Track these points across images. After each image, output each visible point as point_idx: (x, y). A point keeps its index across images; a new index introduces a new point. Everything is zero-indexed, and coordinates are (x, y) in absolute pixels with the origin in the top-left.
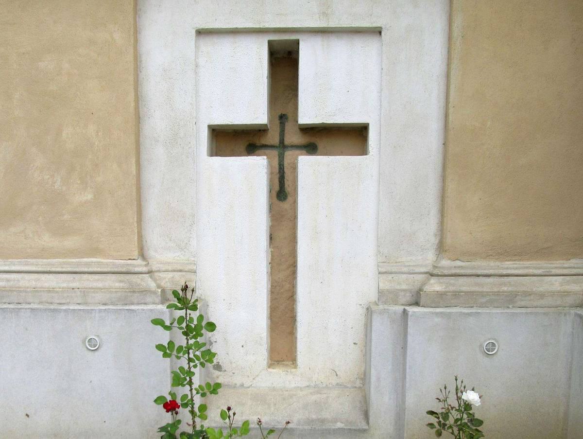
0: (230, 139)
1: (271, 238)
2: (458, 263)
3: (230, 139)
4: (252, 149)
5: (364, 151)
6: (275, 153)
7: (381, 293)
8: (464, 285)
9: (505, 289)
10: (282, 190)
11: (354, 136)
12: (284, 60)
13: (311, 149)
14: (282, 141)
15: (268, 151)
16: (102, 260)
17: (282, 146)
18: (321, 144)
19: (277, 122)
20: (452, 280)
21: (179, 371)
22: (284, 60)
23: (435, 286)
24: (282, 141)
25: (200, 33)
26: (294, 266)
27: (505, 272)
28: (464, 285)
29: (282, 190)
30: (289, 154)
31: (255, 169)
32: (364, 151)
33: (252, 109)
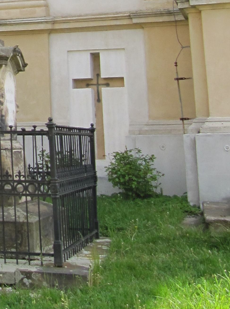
0: (79, 83)
1: (96, 115)
2: (155, 121)
3: (79, 83)
4: (88, 85)
5: (123, 86)
6: (95, 87)
7: (130, 131)
8: (155, 127)
9: (168, 128)
10: (98, 99)
11: (119, 81)
12: (95, 57)
13: (107, 85)
14: (98, 83)
15: (92, 86)
16: (39, 122)
17: (98, 84)
18: (111, 83)
19: (96, 77)
20: (151, 126)
21: (52, 276)
22: (95, 57)
23: (146, 128)
24: (98, 83)
25: (68, 51)
26: (103, 125)
27: (169, 124)
28: (155, 127)
29: (98, 99)
30: (100, 87)
31: (87, 93)
32: (123, 86)
33: (86, 73)
